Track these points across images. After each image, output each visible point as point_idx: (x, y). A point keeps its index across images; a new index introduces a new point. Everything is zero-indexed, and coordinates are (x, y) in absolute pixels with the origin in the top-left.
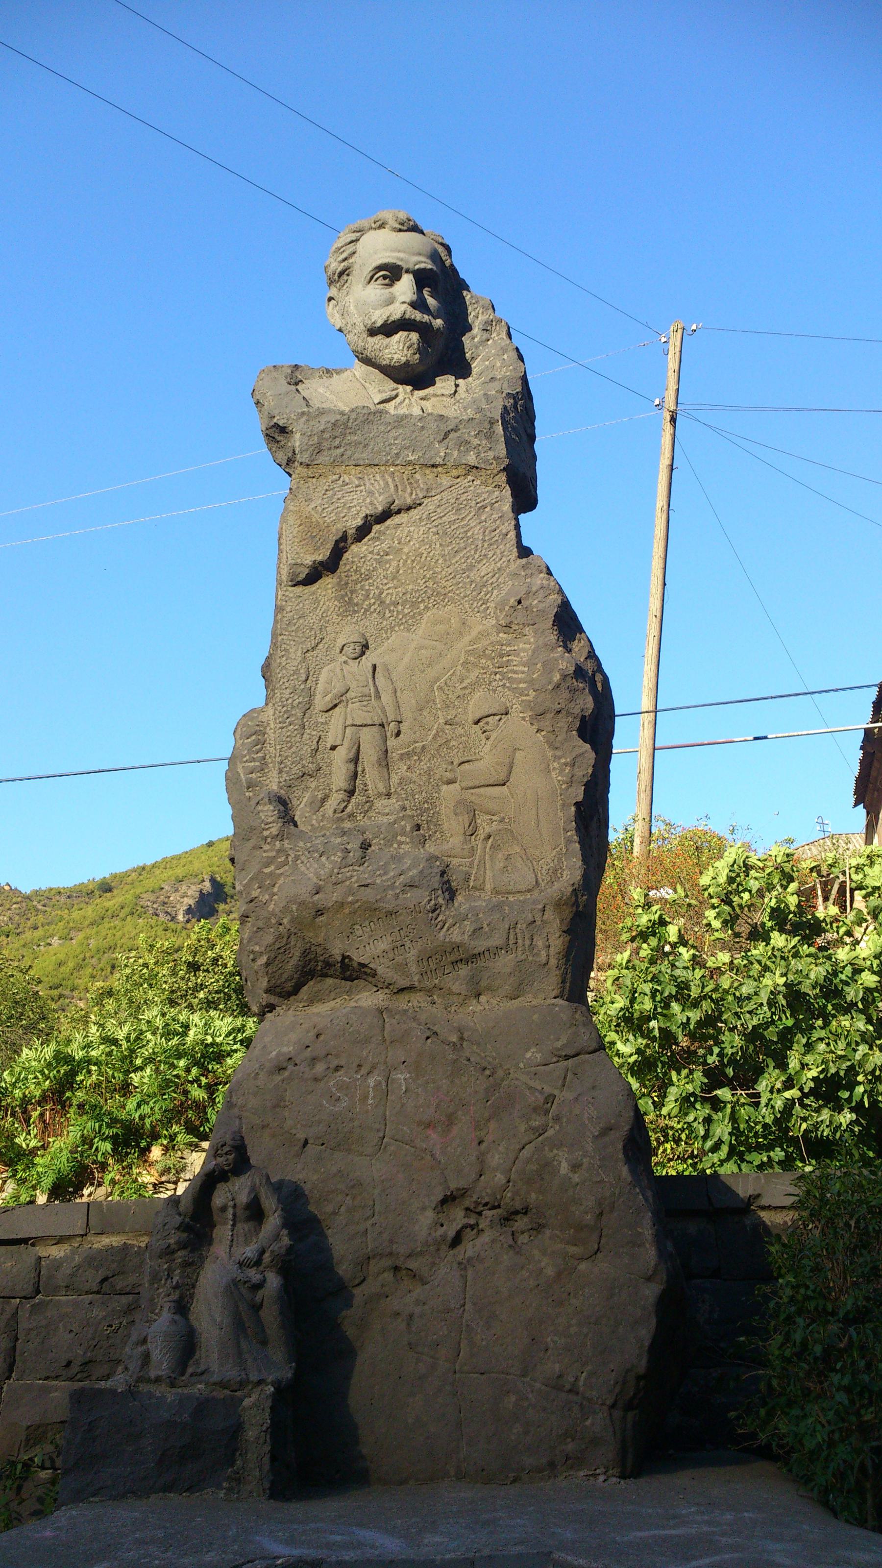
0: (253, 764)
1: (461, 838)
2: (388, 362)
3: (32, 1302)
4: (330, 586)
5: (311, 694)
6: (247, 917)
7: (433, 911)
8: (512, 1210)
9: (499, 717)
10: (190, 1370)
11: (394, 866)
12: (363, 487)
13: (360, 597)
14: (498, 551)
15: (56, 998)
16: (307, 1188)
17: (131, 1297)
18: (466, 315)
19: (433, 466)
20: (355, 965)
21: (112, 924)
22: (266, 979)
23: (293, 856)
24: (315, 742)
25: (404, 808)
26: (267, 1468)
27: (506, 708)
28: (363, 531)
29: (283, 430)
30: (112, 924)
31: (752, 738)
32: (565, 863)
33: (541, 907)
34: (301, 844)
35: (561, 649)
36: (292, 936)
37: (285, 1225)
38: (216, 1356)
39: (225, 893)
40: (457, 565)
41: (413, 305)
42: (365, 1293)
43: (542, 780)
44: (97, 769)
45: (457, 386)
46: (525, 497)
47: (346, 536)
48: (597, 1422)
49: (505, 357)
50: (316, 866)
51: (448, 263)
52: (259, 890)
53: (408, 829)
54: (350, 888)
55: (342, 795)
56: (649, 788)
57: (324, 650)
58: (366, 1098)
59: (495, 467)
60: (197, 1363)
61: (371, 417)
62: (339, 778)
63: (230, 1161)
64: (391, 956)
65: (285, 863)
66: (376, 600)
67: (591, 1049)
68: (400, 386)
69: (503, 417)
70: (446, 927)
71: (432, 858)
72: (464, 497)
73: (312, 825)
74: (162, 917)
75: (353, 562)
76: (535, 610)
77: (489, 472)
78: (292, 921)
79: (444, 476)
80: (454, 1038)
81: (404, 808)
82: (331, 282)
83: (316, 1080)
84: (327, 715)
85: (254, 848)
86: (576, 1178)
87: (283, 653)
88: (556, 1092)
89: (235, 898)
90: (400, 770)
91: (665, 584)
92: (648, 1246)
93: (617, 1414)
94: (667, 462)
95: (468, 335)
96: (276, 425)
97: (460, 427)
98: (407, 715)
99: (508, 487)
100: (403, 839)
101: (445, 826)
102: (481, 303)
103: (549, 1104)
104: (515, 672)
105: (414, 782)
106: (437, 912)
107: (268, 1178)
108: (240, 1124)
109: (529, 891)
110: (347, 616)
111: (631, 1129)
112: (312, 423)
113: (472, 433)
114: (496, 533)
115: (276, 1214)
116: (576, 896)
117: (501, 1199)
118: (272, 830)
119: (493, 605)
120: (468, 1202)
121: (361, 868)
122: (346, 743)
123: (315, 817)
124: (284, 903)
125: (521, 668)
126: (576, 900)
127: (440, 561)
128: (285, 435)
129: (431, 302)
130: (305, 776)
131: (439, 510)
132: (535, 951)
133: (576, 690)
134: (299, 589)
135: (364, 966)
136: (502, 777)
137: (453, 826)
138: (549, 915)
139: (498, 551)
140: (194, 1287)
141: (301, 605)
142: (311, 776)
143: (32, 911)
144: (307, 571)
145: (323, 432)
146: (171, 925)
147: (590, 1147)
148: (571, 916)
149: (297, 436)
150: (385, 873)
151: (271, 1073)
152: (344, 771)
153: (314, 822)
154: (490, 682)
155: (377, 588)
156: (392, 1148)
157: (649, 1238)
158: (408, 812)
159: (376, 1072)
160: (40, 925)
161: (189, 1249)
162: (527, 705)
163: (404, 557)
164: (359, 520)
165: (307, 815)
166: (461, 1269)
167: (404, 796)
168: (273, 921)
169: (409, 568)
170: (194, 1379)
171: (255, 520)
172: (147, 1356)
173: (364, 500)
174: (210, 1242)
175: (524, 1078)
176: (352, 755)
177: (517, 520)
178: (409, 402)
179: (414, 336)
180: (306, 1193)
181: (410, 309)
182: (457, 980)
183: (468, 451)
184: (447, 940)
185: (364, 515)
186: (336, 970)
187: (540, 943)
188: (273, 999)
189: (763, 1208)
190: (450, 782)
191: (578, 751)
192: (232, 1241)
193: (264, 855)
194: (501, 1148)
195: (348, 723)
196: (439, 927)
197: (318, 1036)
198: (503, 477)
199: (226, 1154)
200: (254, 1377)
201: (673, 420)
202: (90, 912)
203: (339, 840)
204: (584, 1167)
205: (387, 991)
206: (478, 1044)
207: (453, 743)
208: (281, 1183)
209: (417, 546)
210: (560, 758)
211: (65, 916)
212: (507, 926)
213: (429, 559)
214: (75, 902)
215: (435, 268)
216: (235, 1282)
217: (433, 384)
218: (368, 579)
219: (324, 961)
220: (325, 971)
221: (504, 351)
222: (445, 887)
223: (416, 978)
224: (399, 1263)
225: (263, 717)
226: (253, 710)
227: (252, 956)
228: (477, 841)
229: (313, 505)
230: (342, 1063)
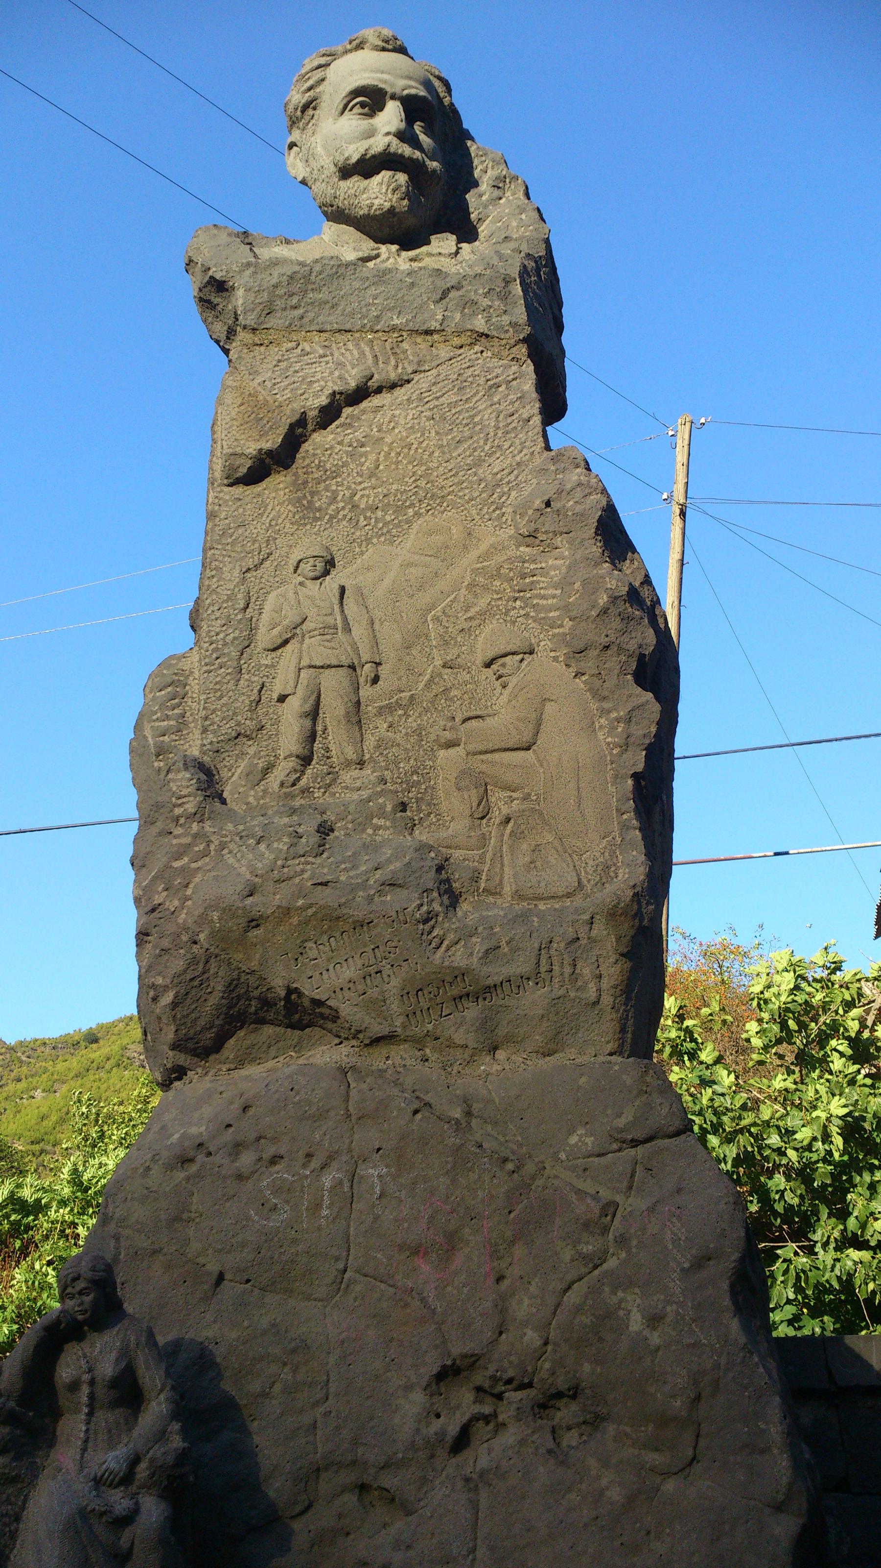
0: (166, 723)
1: (467, 822)
2: (365, 211)
4: (281, 486)
5: (252, 630)
6: (147, 935)
7: (425, 921)
8: (553, 1391)
9: (521, 656)
11: (367, 858)
13: (324, 500)
14: (517, 442)
15: (38, 1153)
16: (219, 1353)
20: (306, 1003)
21: (97, 1076)
22: (173, 1028)
23: (217, 843)
24: (256, 691)
27: (531, 645)
28: (329, 414)
29: (220, 286)
30: (97, 1076)
31: (772, 854)
32: (620, 857)
33: (586, 917)
35: (607, 564)
36: (212, 960)
37: (175, 1415)
40: (459, 459)
41: (400, 136)
42: (311, 1527)
44: (17, 829)
47: (306, 420)
49: (523, 216)
50: (250, 856)
51: (446, 101)
52: (165, 893)
53: (389, 808)
54: (301, 887)
55: (293, 763)
57: (272, 569)
58: (318, 1206)
59: (511, 336)
61: (342, 270)
62: (289, 739)
63: (87, 1306)
64: (361, 987)
65: (205, 854)
66: (347, 504)
67: (672, 1129)
69: (521, 276)
70: (444, 946)
71: (423, 848)
72: (469, 372)
73: (247, 804)
75: (314, 455)
76: (570, 514)
77: (504, 342)
78: (212, 935)
79: (442, 345)
80: (457, 1113)
82: (293, 122)
83: (240, 1177)
84: (274, 654)
85: (160, 834)
87: (214, 572)
88: (619, 1198)
90: (377, 729)
92: (776, 1451)
95: (473, 192)
97: (464, 283)
98: (389, 655)
99: (529, 361)
100: (381, 822)
101: (444, 806)
102: (490, 156)
103: (609, 1218)
104: (543, 597)
105: (398, 745)
106: (432, 922)
107: (151, 1334)
108: (117, 1248)
109: (568, 895)
110: (305, 525)
111: (742, 1260)
112: (259, 277)
113: (481, 291)
114: (514, 417)
115: (162, 1397)
116: (639, 903)
117: (534, 1373)
118: (186, 806)
119: (510, 510)
120: (480, 1378)
121: (318, 860)
122: (300, 692)
123: (252, 793)
124: (201, 910)
125: (551, 591)
126: (640, 909)
127: (436, 454)
128: (224, 294)
130: (241, 738)
131: (434, 389)
132: (579, 983)
133: (630, 619)
134: (239, 490)
136: (527, 737)
138: (599, 929)
139: (517, 442)
140: (18, 1518)
141: (241, 510)
142: (249, 737)
143: (16, 1062)
144: (249, 463)
145: (275, 286)
148: (632, 932)
149: (240, 293)
150: (354, 867)
151: (169, 1167)
152: (297, 730)
154: (507, 611)
155: (348, 488)
156: (358, 1288)
159: (335, 1165)
160: (23, 1077)
161: (12, 1454)
163: (386, 449)
164: (324, 398)
165: (241, 790)
166: (470, 1490)
167: (383, 764)
168: (185, 938)
169: (391, 463)
173: (331, 373)
174: (51, 1443)
175: (566, 1175)
176: (308, 707)
179: (402, 178)
180: (218, 1360)
181: (395, 142)
182: (462, 1024)
183: (474, 314)
184: (446, 964)
185: (330, 391)
186: (277, 1013)
187: (586, 971)
188: (183, 1059)
190: (451, 744)
192: (86, 1441)
193: (175, 842)
194: (533, 1289)
195: (303, 664)
196: (433, 945)
197: (245, 1109)
198: (523, 350)
199: (80, 1293)
201: (683, 514)
202: (74, 1064)
203: (286, 820)
204: (668, 1320)
205: (354, 1042)
206: (496, 1123)
208: (177, 1346)
209: (404, 434)
210: (609, 712)
211: (50, 1068)
212: (536, 945)
213: (420, 451)
214: (60, 1053)
215: (430, 98)
216: (84, 1514)
218: (335, 477)
219: (259, 998)
220: (261, 1014)
222: (443, 887)
225: (186, 665)
226: (171, 657)
227: (152, 993)
228: (491, 828)
229: (259, 379)
230: (282, 1151)
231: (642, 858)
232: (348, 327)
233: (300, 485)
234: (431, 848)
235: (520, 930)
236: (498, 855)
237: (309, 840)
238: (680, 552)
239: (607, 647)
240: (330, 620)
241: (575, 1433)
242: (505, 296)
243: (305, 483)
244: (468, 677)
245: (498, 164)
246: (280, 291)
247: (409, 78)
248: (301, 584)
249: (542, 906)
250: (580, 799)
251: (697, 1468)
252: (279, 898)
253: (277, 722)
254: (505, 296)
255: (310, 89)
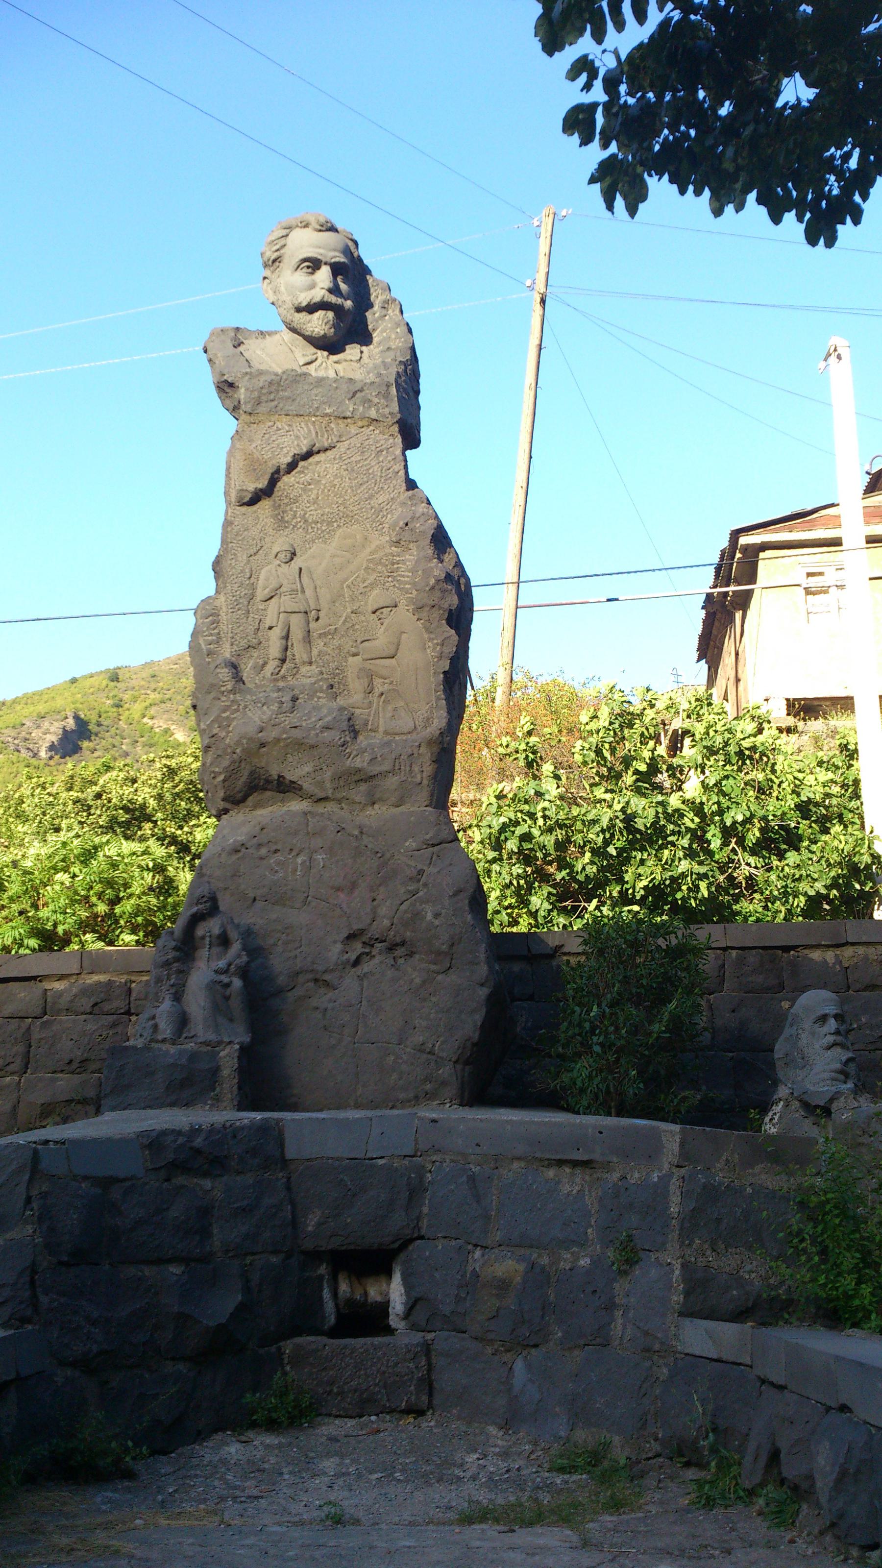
1: (362, 695)
3: (41, 1020)
5: (253, 587)
7: (343, 746)
10: (184, 1035)
12: (291, 433)
17: (115, 1016)
18: (369, 294)
19: (344, 418)
20: (287, 782)
22: (223, 791)
25: (322, 673)
26: (236, 1093)
28: (292, 466)
29: (231, 385)
33: (417, 744)
34: (249, 697)
38: (201, 1026)
39: (89, 730)
41: (330, 291)
43: (420, 657)
45: (362, 352)
46: (411, 439)
48: (446, 1071)
49: (398, 330)
51: (355, 255)
53: (325, 688)
55: (277, 662)
56: (511, 644)
58: (296, 870)
59: (390, 420)
60: (189, 1031)
61: (298, 378)
62: (274, 649)
64: (313, 776)
65: (237, 710)
68: (319, 352)
69: (396, 381)
71: (342, 709)
72: (367, 443)
74: (24, 754)
80: (356, 832)
81: (322, 673)
83: (261, 858)
84: (266, 603)
85: (214, 698)
86: (437, 922)
88: (425, 868)
89: (100, 735)
90: (319, 646)
91: (531, 457)
93: (459, 1067)
94: (537, 342)
95: (370, 311)
96: (226, 381)
98: (324, 605)
99: (399, 436)
100: (321, 695)
101: (351, 687)
104: (403, 576)
107: (232, 919)
109: (409, 733)
111: (475, 891)
113: (374, 394)
121: (292, 715)
122: (280, 625)
125: (407, 574)
129: (343, 287)
131: (348, 452)
134: (244, 509)
135: (294, 782)
136: (392, 652)
137: (356, 686)
138: (423, 750)
144: (250, 496)
145: (262, 388)
146: (34, 762)
147: (446, 902)
149: (242, 390)
150: (309, 719)
151: (230, 854)
153: (257, 681)
157: (483, 959)
158: (325, 676)
159: (302, 854)
162: (411, 601)
168: (229, 751)
170: (186, 1041)
171: (203, 448)
172: (156, 1027)
174: (194, 960)
176: (284, 634)
177: (404, 455)
178: (326, 366)
179: (330, 315)
181: (327, 293)
182: (359, 793)
183: (370, 407)
187: (416, 769)
189: (565, 954)
190: (355, 655)
191: (446, 635)
194: (387, 903)
198: (396, 428)
200: (226, 1040)
201: (543, 301)
203: (276, 695)
206: (373, 837)
207: (357, 627)
210: (433, 639)
217: (344, 350)
221: (398, 325)
223: (330, 792)
224: (318, 976)
225: (217, 603)
227: (213, 775)
231: (445, 714)
232: (302, 413)
233: (277, 507)
234: (345, 709)
235: (386, 750)
236: (377, 713)
237: (287, 706)
238: (539, 338)
239: (433, 606)
240: (294, 587)
241: (403, 959)
242: (387, 396)
243: (279, 506)
244: (363, 618)
245: (385, 290)
246: (264, 391)
247: (335, 250)
248: (279, 565)
249: (397, 738)
250: (417, 683)
251: (451, 970)
252: (274, 734)
253: (268, 640)
254: (387, 396)
255: (277, 250)
